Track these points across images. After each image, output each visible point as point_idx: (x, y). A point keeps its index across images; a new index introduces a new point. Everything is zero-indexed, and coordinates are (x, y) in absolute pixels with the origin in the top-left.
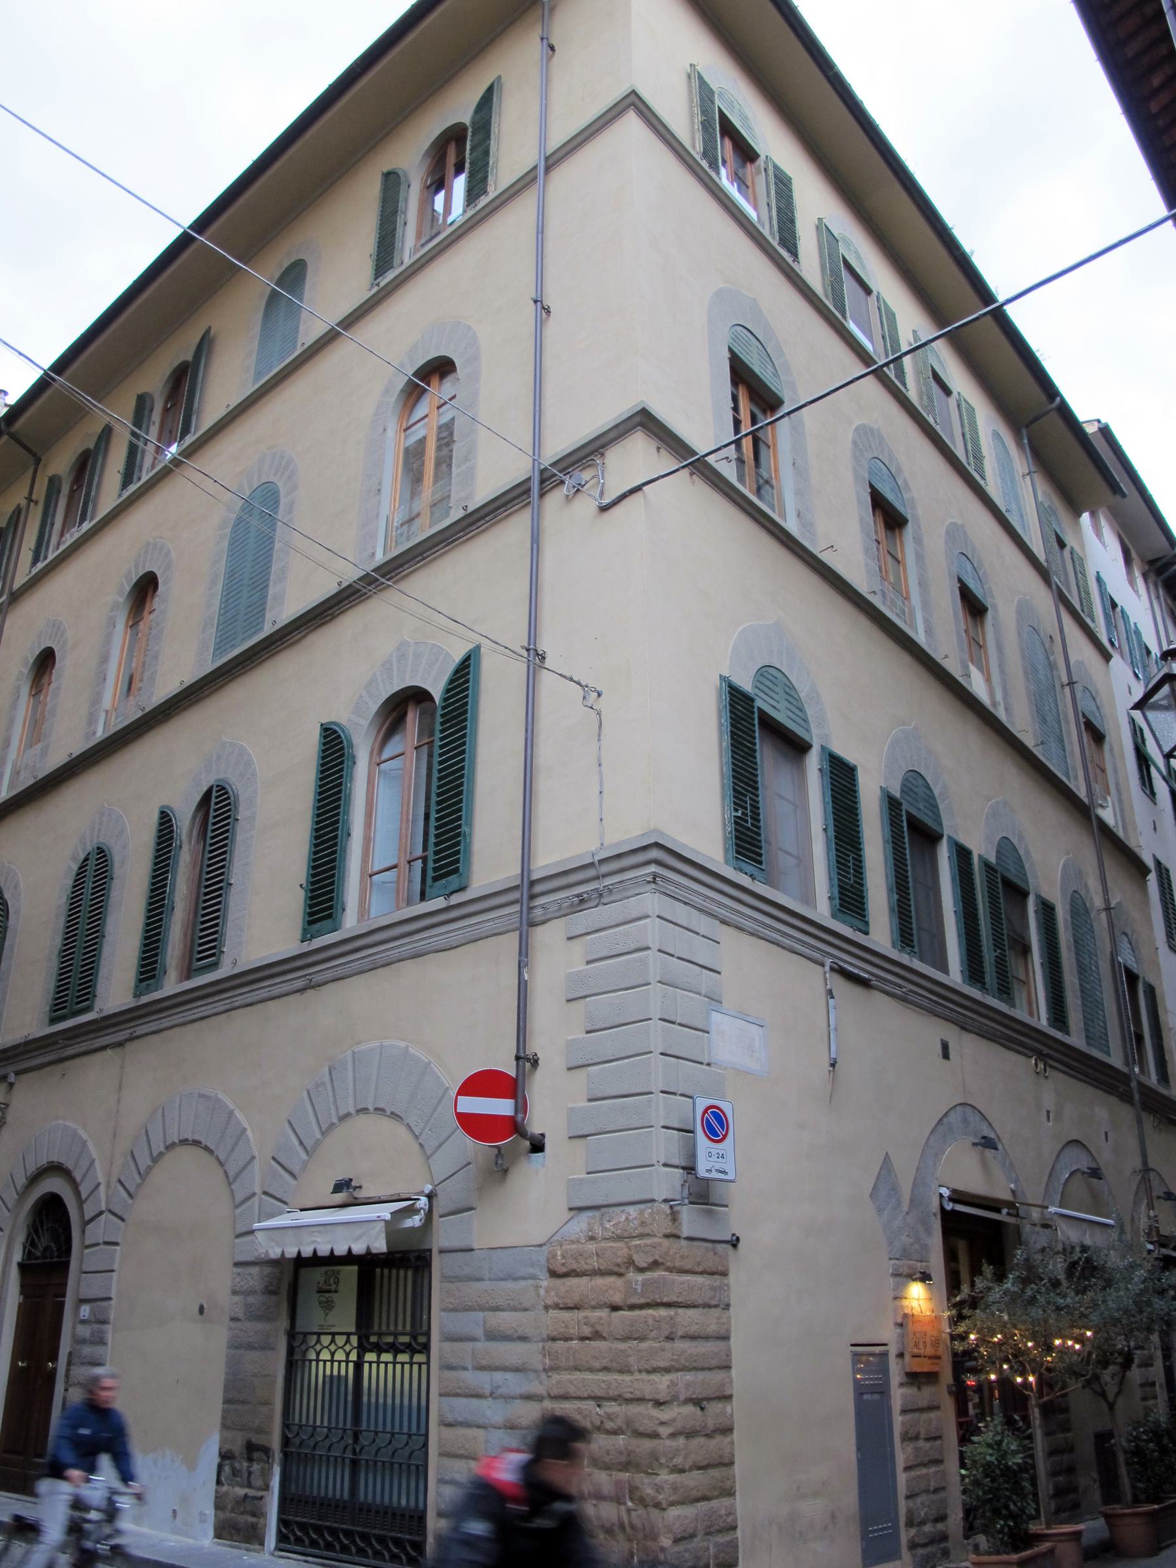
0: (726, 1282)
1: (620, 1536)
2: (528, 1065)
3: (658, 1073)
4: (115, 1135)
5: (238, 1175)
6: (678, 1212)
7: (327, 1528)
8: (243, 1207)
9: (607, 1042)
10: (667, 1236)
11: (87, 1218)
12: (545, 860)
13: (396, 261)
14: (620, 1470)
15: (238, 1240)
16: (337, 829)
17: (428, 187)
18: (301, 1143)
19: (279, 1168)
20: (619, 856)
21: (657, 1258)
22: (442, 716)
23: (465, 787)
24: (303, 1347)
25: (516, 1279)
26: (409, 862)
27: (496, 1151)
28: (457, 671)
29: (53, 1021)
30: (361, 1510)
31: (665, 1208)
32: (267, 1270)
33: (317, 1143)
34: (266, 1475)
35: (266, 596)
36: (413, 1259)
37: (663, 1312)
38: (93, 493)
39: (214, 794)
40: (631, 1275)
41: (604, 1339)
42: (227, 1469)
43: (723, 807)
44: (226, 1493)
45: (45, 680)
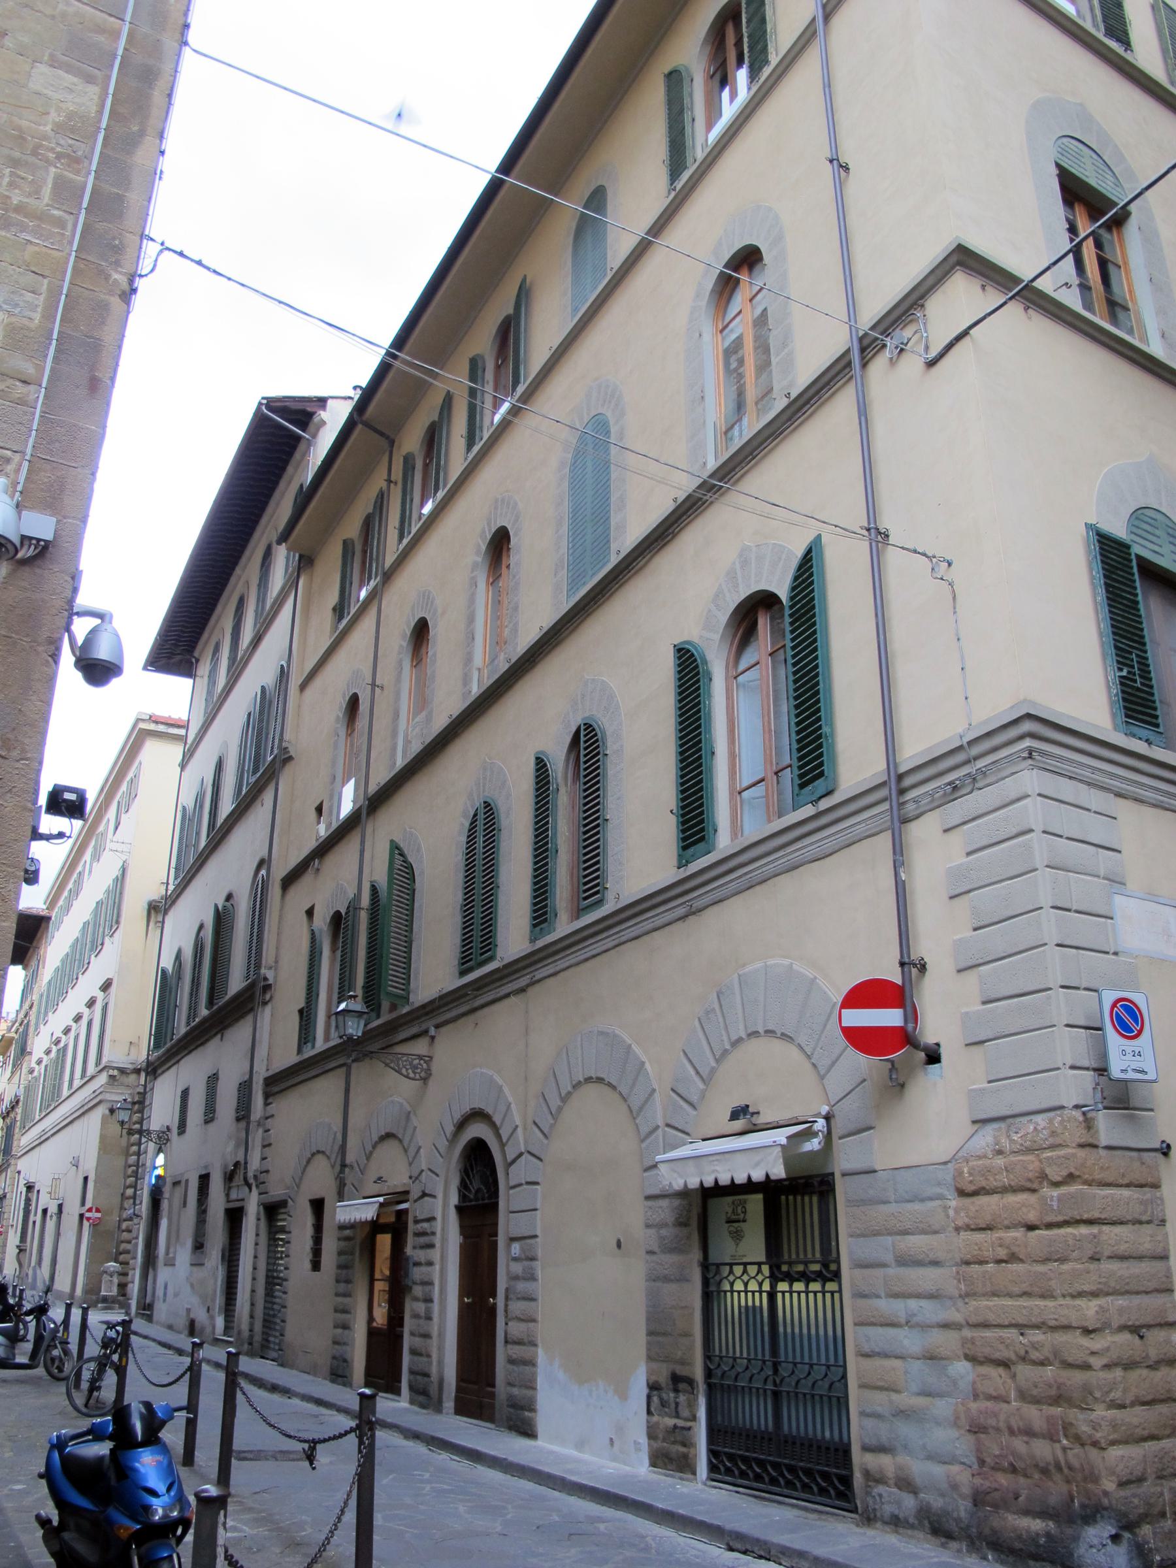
0: (1158, 1194)
1: (1057, 1477)
2: (914, 971)
3: (1055, 966)
4: (526, 1078)
5: (641, 1109)
6: (1093, 1119)
7: (755, 1459)
8: (648, 1141)
9: (997, 939)
10: (1082, 1146)
11: (509, 1159)
12: (911, 751)
13: (689, 160)
14: (1051, 1405)
15: (646, 1174)
16: (700, 750)
17: (712, 77)
18: (698, 1073)
19: (678, 1099)
20: (989, 735)
21: (1073, 1170)
22: (791, 616)
23: (821, 686)
24: (717, 1278)
25: (922, 1200)
26: (776, 773)
27: (889, 1065)
28: (800, 567)
29: (463, 973)
30: (786, 1442)
31: (1077, 1114)
32: (677, 1202)
33: (713, 1071)
34: (692, 1405)
35: (609, 528)
36: (816, 1184)
37: (1084, 1230)
38: (442, 462)
39: (582, 733)
40: (1046, 1191)
41: (1022, 1261)
42: (655, 1399)
43: (1106, 669)
44: (657, 1423)
45: (423, 650)
